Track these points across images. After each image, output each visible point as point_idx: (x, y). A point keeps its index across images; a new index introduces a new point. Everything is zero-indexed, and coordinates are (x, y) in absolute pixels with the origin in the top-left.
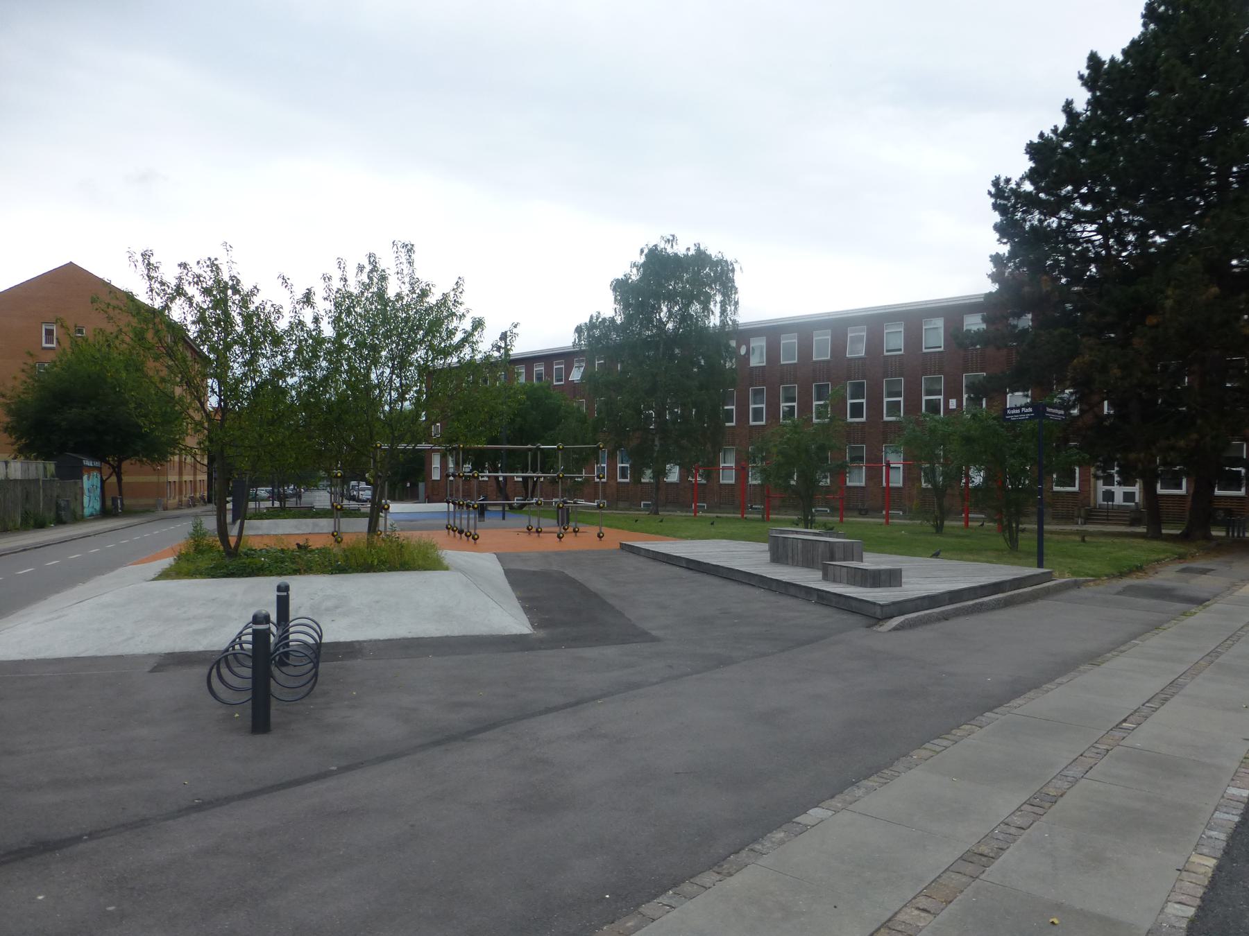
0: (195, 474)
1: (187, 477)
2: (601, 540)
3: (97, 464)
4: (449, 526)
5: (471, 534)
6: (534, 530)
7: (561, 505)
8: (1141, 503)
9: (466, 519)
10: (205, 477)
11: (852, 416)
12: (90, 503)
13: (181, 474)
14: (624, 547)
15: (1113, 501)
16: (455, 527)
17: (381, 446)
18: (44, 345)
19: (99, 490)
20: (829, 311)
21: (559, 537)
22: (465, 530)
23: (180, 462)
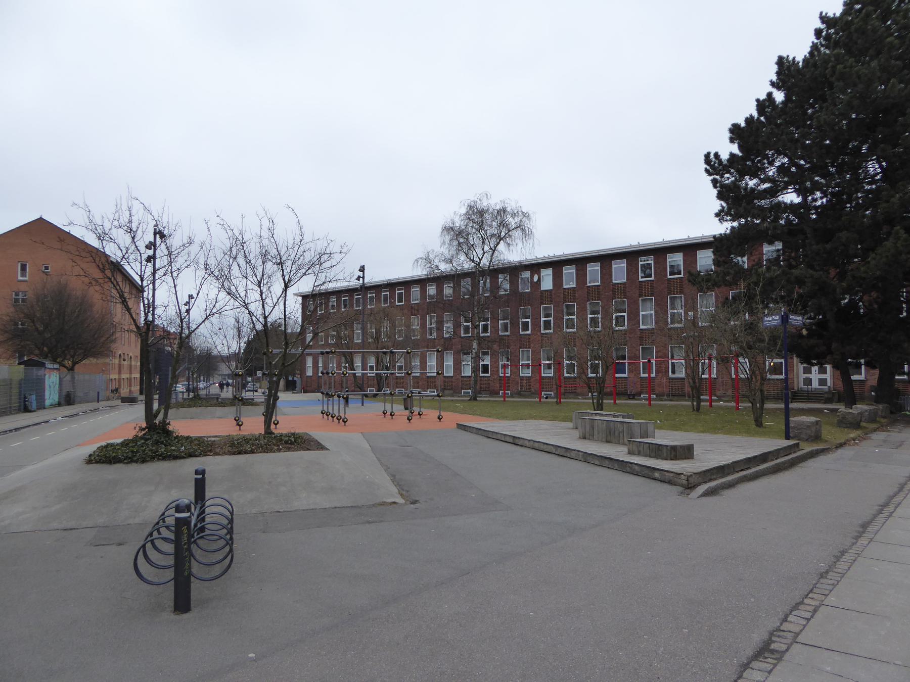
0: (131, 373)
1: (125, 376)
2: (440, 421)
3: (56, 366)
4: (324, 412)
5: (330, 413)
6: (388, 413)
7: (410, 395)
8: (832, 387)
9: (335, 406)
10: (138, 375)
11: (545, 329)
12: (51, 395)
13: (120, 373)
14: (461, 427)
15: (811, 386)
16: (328, 412)
17: (272, 351)
18: (20, 278)
19: (57, 386)
20: (598, 249)
21: (408, 419)
22: (337, 415)
23: (120, 365)
